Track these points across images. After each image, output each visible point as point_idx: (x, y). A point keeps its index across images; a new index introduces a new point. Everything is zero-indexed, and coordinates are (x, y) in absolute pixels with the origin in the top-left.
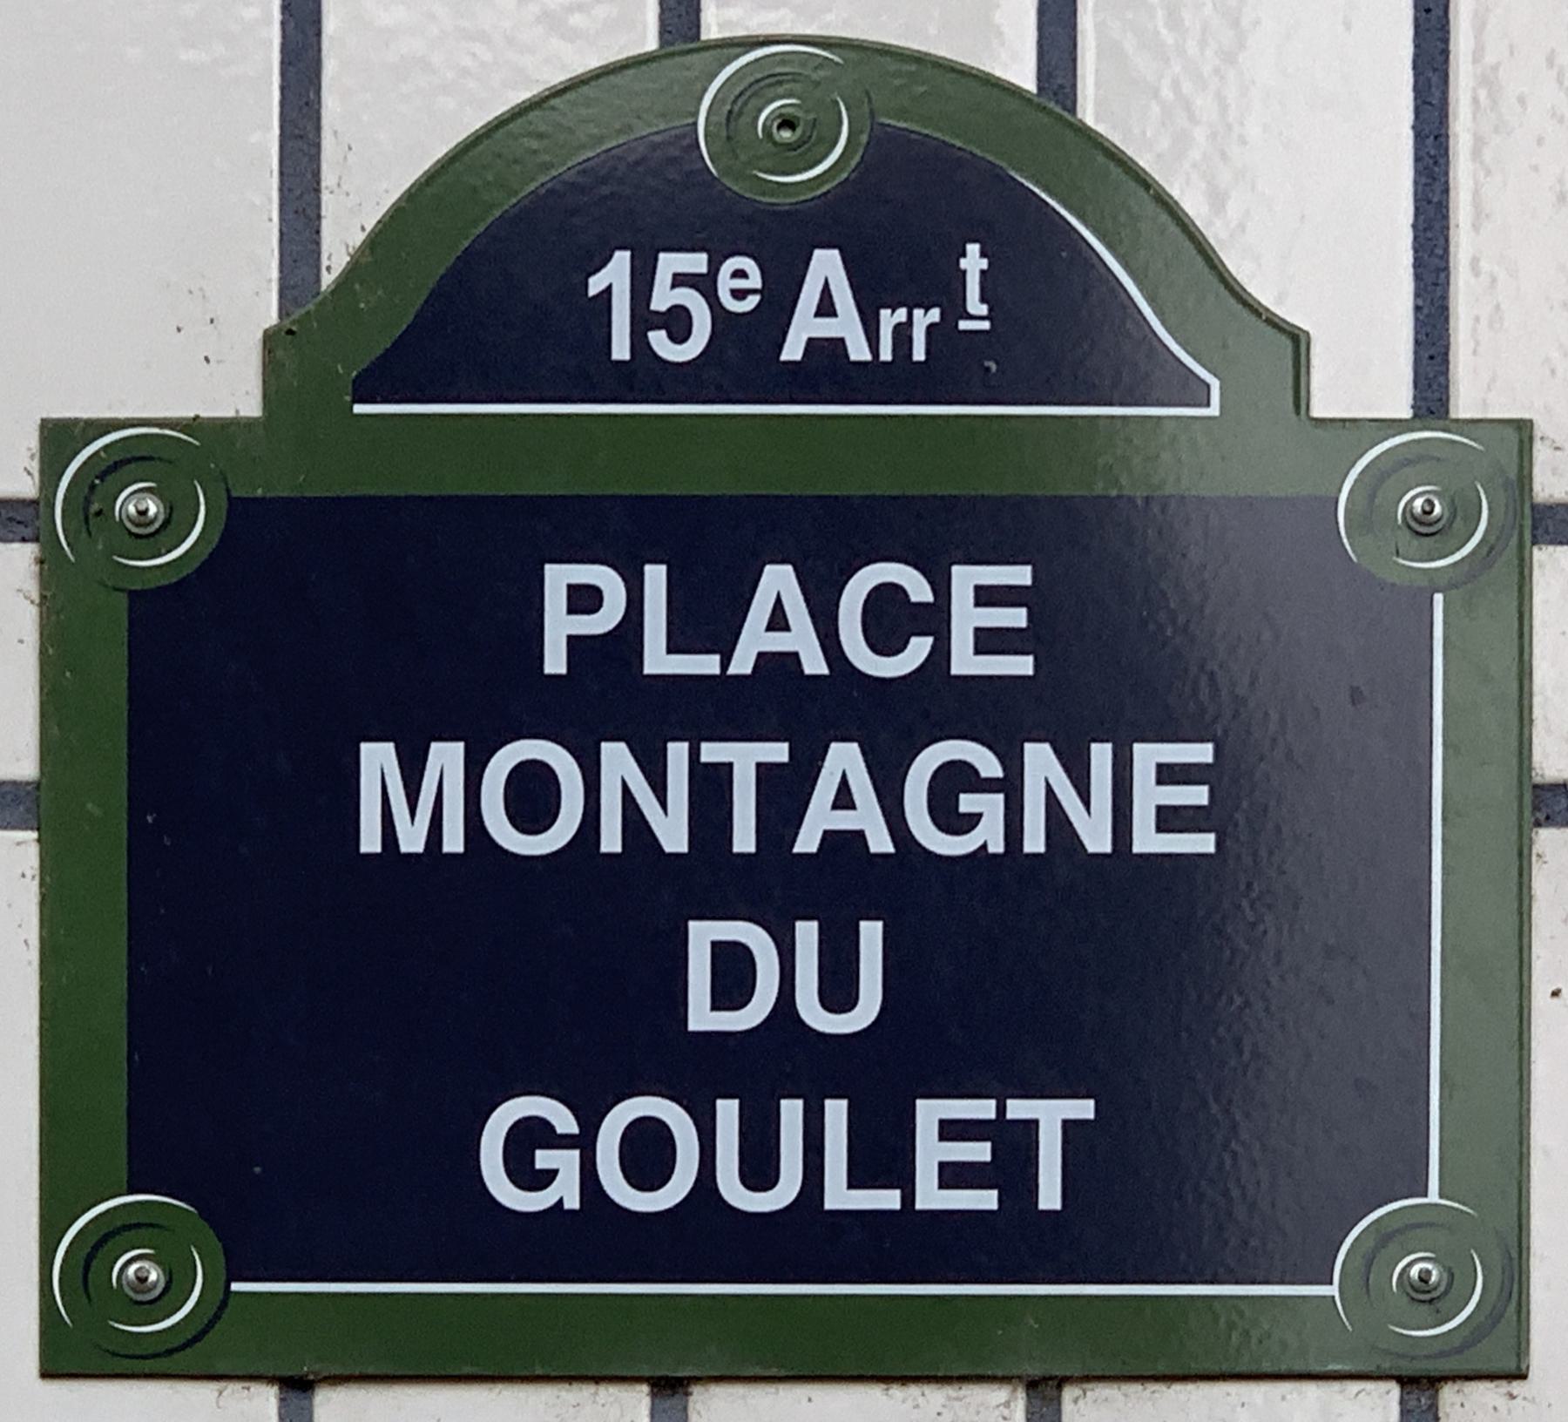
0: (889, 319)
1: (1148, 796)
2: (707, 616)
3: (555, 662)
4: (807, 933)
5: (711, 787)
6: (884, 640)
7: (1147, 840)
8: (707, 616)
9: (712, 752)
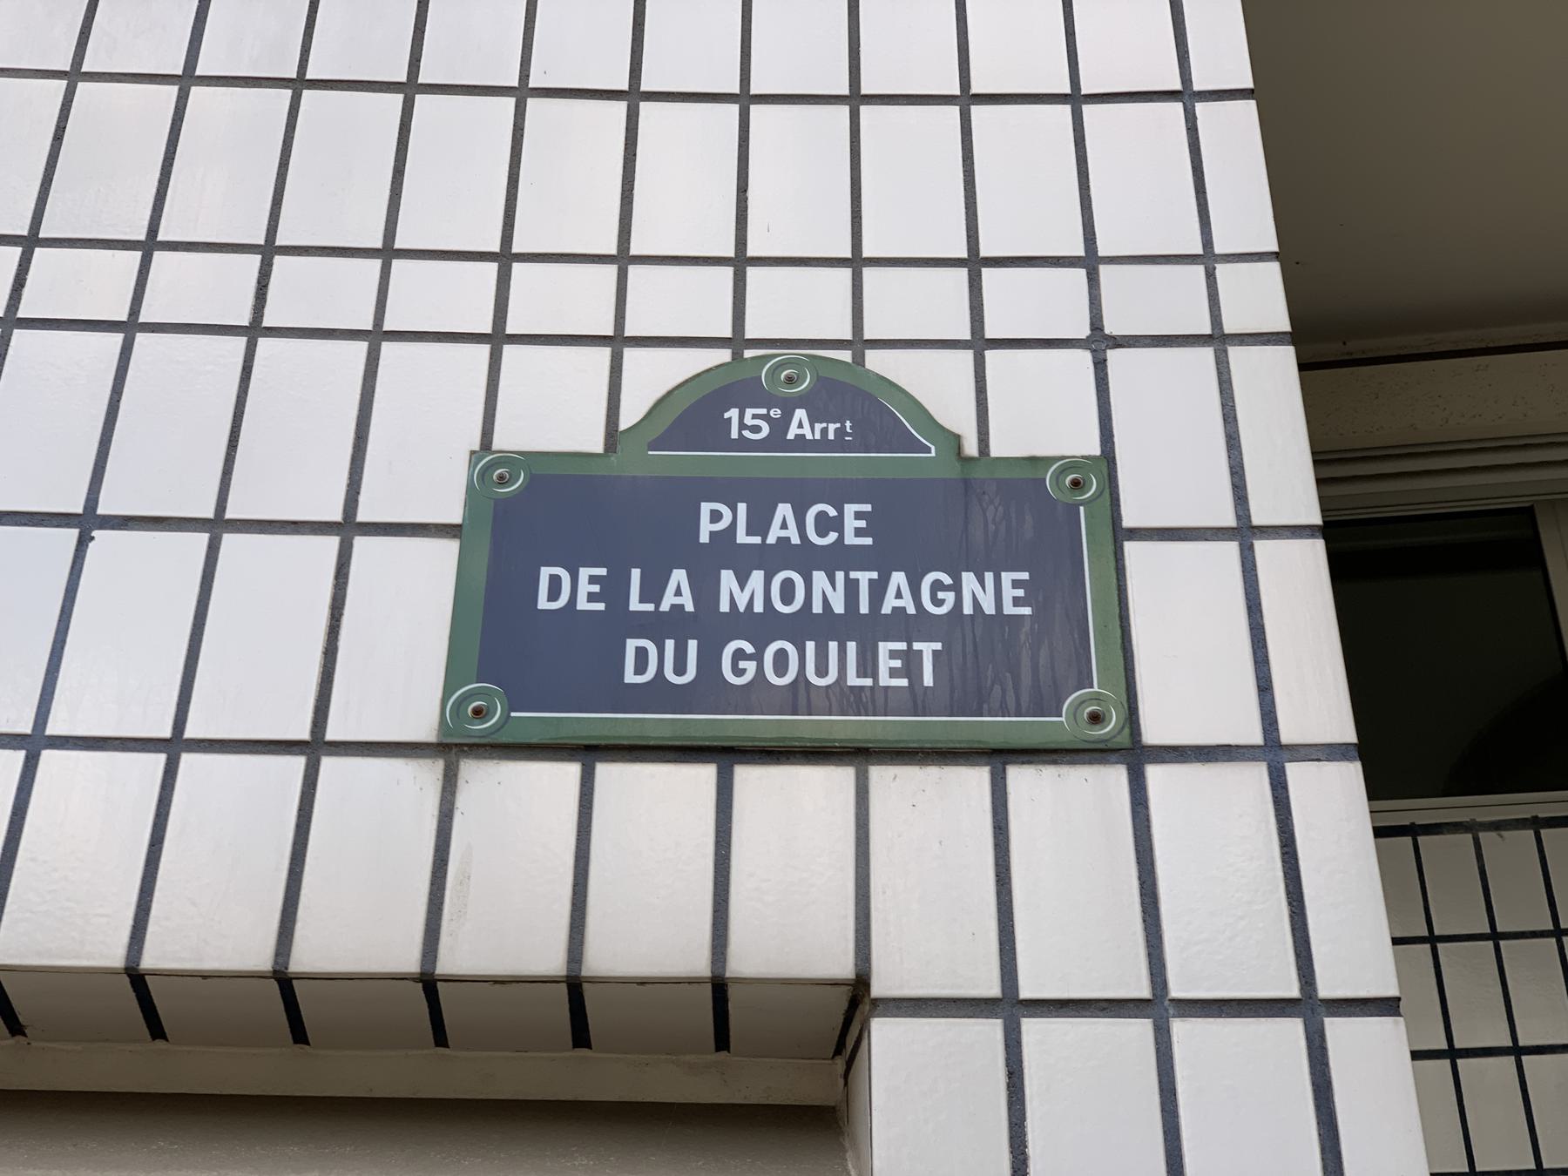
0: (818, 427)
1: (1009, 593)
2: (758, 524)
3: (704, 538)
4: (810, 646)
5: (852, 588)
6: (821, 533)
7: (1009, 609)
8: (758, 524)
9: (853, 575)
